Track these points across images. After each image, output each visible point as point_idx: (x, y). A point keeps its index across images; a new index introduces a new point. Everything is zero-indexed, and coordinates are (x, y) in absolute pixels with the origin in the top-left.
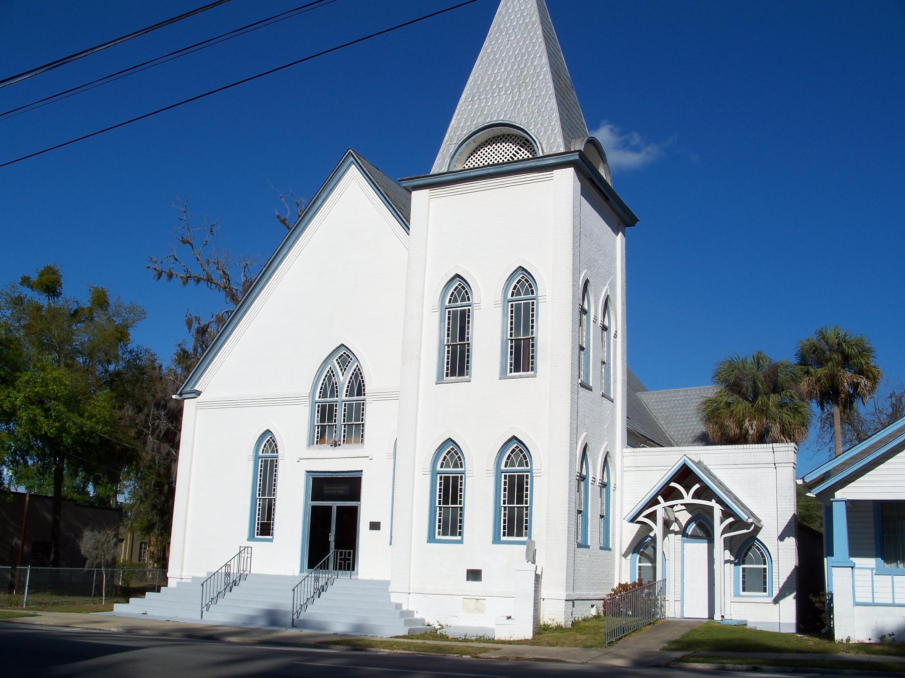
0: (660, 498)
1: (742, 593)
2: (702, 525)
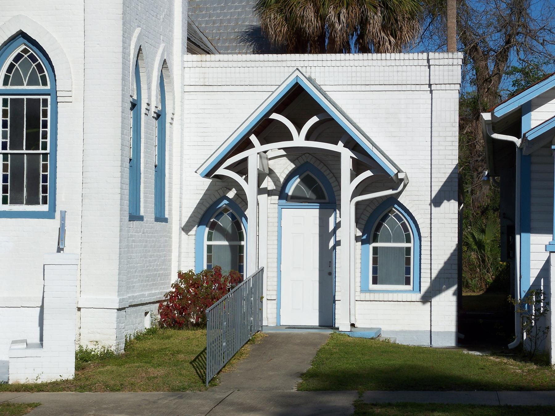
0: (253, 138)
1: (372, 287)
2: (315, 183)
